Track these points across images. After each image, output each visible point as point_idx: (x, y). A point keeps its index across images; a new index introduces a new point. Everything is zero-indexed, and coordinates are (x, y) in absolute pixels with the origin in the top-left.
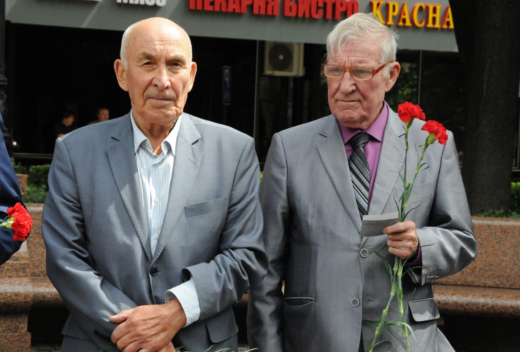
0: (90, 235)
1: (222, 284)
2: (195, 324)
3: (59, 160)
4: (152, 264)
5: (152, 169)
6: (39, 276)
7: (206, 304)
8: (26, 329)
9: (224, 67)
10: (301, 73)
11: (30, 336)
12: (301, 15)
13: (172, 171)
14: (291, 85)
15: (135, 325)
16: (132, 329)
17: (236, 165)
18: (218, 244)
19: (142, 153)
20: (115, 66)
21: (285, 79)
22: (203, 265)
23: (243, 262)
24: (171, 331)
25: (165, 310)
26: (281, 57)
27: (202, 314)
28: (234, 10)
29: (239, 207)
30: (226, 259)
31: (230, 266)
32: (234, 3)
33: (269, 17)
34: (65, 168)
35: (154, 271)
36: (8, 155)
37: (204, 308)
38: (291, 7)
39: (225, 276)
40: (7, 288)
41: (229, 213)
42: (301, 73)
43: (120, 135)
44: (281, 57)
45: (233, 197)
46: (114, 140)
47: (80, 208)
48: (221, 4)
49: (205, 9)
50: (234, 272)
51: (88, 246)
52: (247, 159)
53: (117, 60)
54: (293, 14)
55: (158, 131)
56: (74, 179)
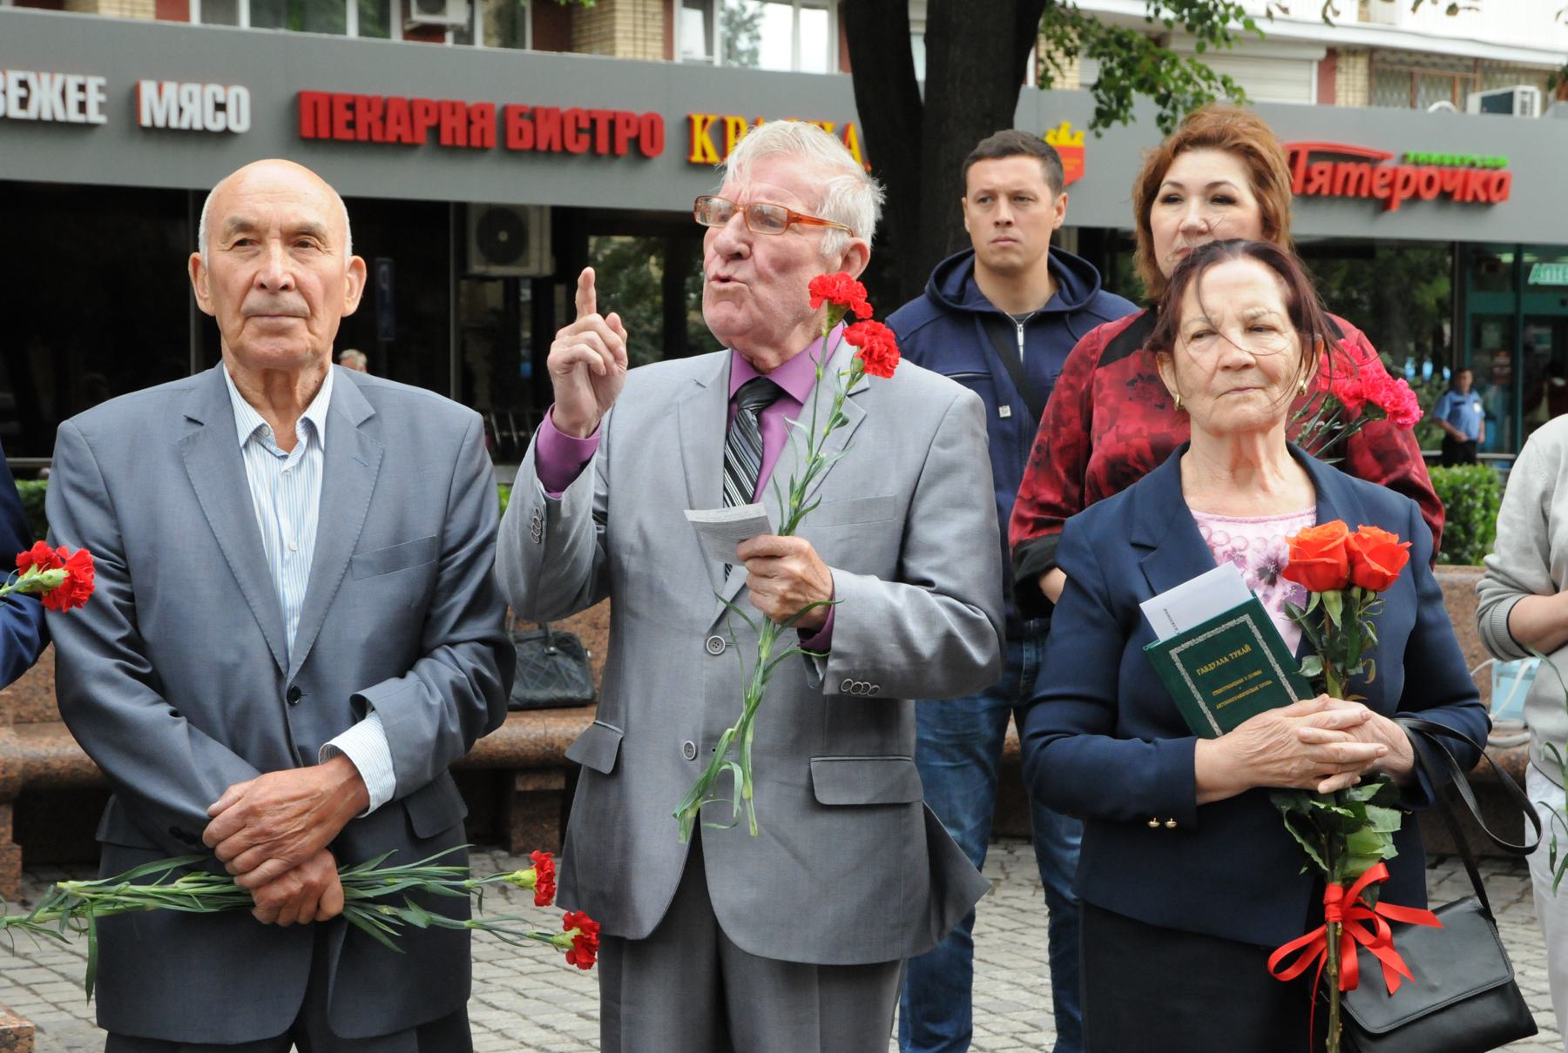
2: (386, 807)
6: (31, 722)
7: (405, 767)
8: (9, 837)
9: (379, 259)
10: (547, 269)
11: (19, 853)
12: (542, 146)
13: (280, 482)
14: (526, 294)
16: (250, 820)
19: (255, 449)
20: (190, 268)
21: (512, 285)
22: (393, 683)
23: (477, 673)
25: (319, 779)
26: (503, 236)
28: (399, 138)
29: (463, 554)
32: (399, 123)
34: (89, 488)
36: (592, 466)
38: (521, 131)
40: (529, 729)
42: (547, 269)
44: (503, 236)
45: (448, 535)
47: (126, 571)
48: (370, 126)
49: (337, 136)
50: (458, 692)
53: (194, 255)
54: (527, 143)
56: (108, 507)
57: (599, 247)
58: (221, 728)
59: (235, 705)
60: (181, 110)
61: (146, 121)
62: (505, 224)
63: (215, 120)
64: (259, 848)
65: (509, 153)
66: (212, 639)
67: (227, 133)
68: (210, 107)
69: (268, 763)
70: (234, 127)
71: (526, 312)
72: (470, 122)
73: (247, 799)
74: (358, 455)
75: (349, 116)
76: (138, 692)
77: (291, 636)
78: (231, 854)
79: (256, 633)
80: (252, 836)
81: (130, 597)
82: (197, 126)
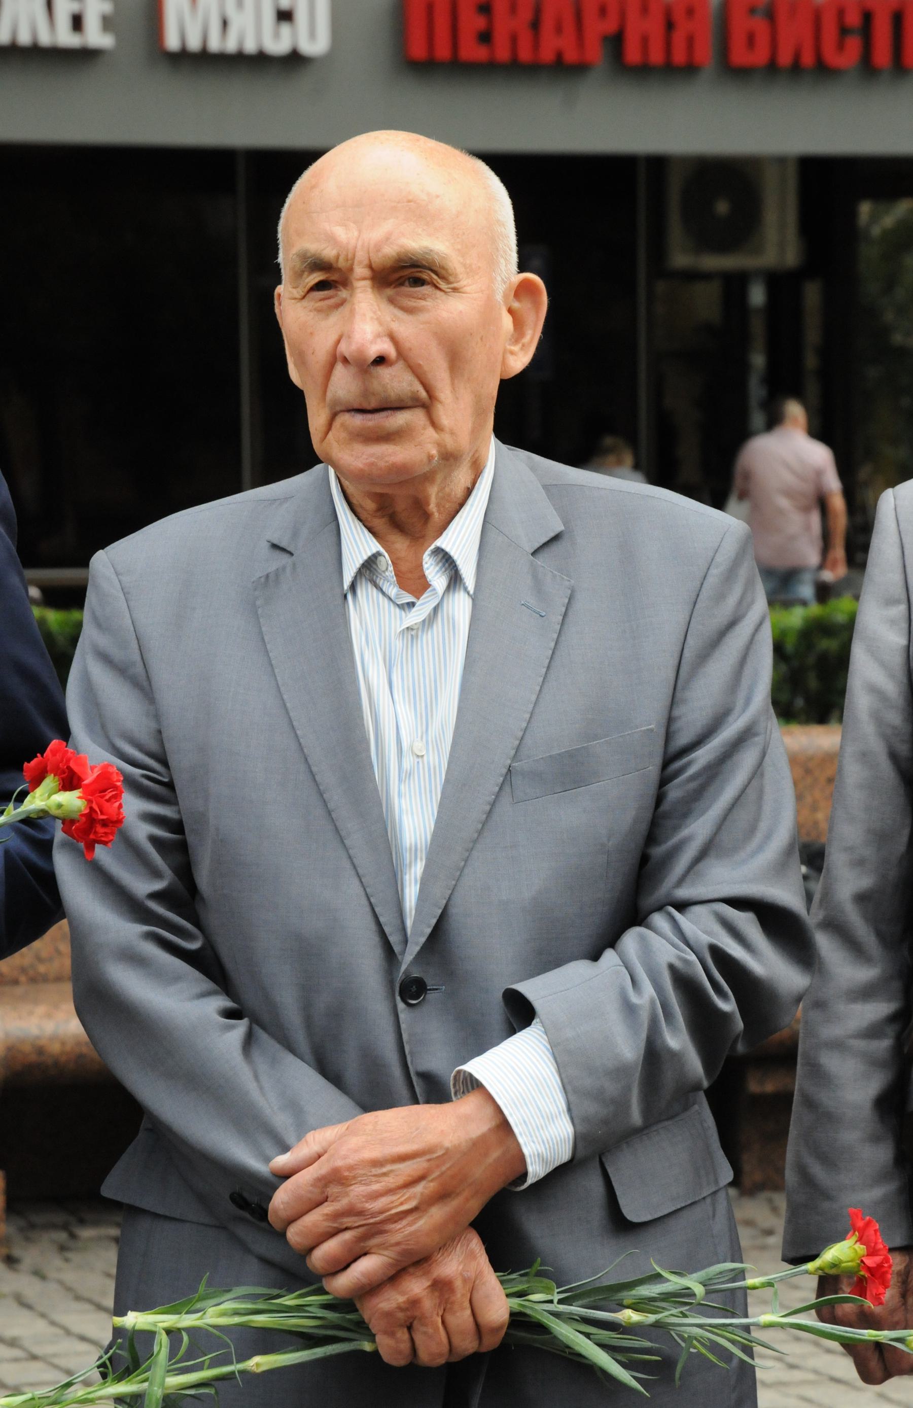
0: (203, 878)
1: (644, 1035)
2: (560, 1174)
3: (99, 625)
4: (403, 968)
5: (398, 644)
7: (591, 1108)
12: (785, 58)
14: (757, 296)
15: (346, 1178)
16: (333, 1190)
17: (682, 617)
18: (635, 892)
19: (365, 592)
21: (735, 285)
23: (717, 953)
24: (467, 1200)
26: (722, 207)
27: (579, 1140)
28: (559, 56)
29: (702, 756)
30: (656, 945)
31: (671, 967)
32: (559, 29)
33: (675, 70)
34: (117, 654)
35: (412, 990)
37: (586, 1119)
39: (652, 1002)
41: (664, 781)
43: (295, 534)
44: (722, 207)
45: (676, 726)
46: (277, 553)
47: (170, 786)
50: (685, 983)
51: (188, 910)
52: (720, 597)
54: (760, 56)
55: (404, 512)
56: (143, 685)
57: (874, 218)
58: (300, 1038)
59: (322, 1002)
60: (225, 24)
61: (172, 42)
62: (726, 182)
63: (277, 35)
64: (347, 1236)
65: (735, 72)
66: (297, 890)
67: (295, 60)
68: (269, 16)
69: (372, 1097)
70: (308, 48)
71: (758, 327)
72: (670, 25)
73: (338, 1151)
74: (532, 601)
75: (480, 22)
76: (177, 978)
77: (411, 895)
78: (307, 1243)
79: (353, 888)
80: (337, 1215)
81: (177, 826)
82: (250, 47)
